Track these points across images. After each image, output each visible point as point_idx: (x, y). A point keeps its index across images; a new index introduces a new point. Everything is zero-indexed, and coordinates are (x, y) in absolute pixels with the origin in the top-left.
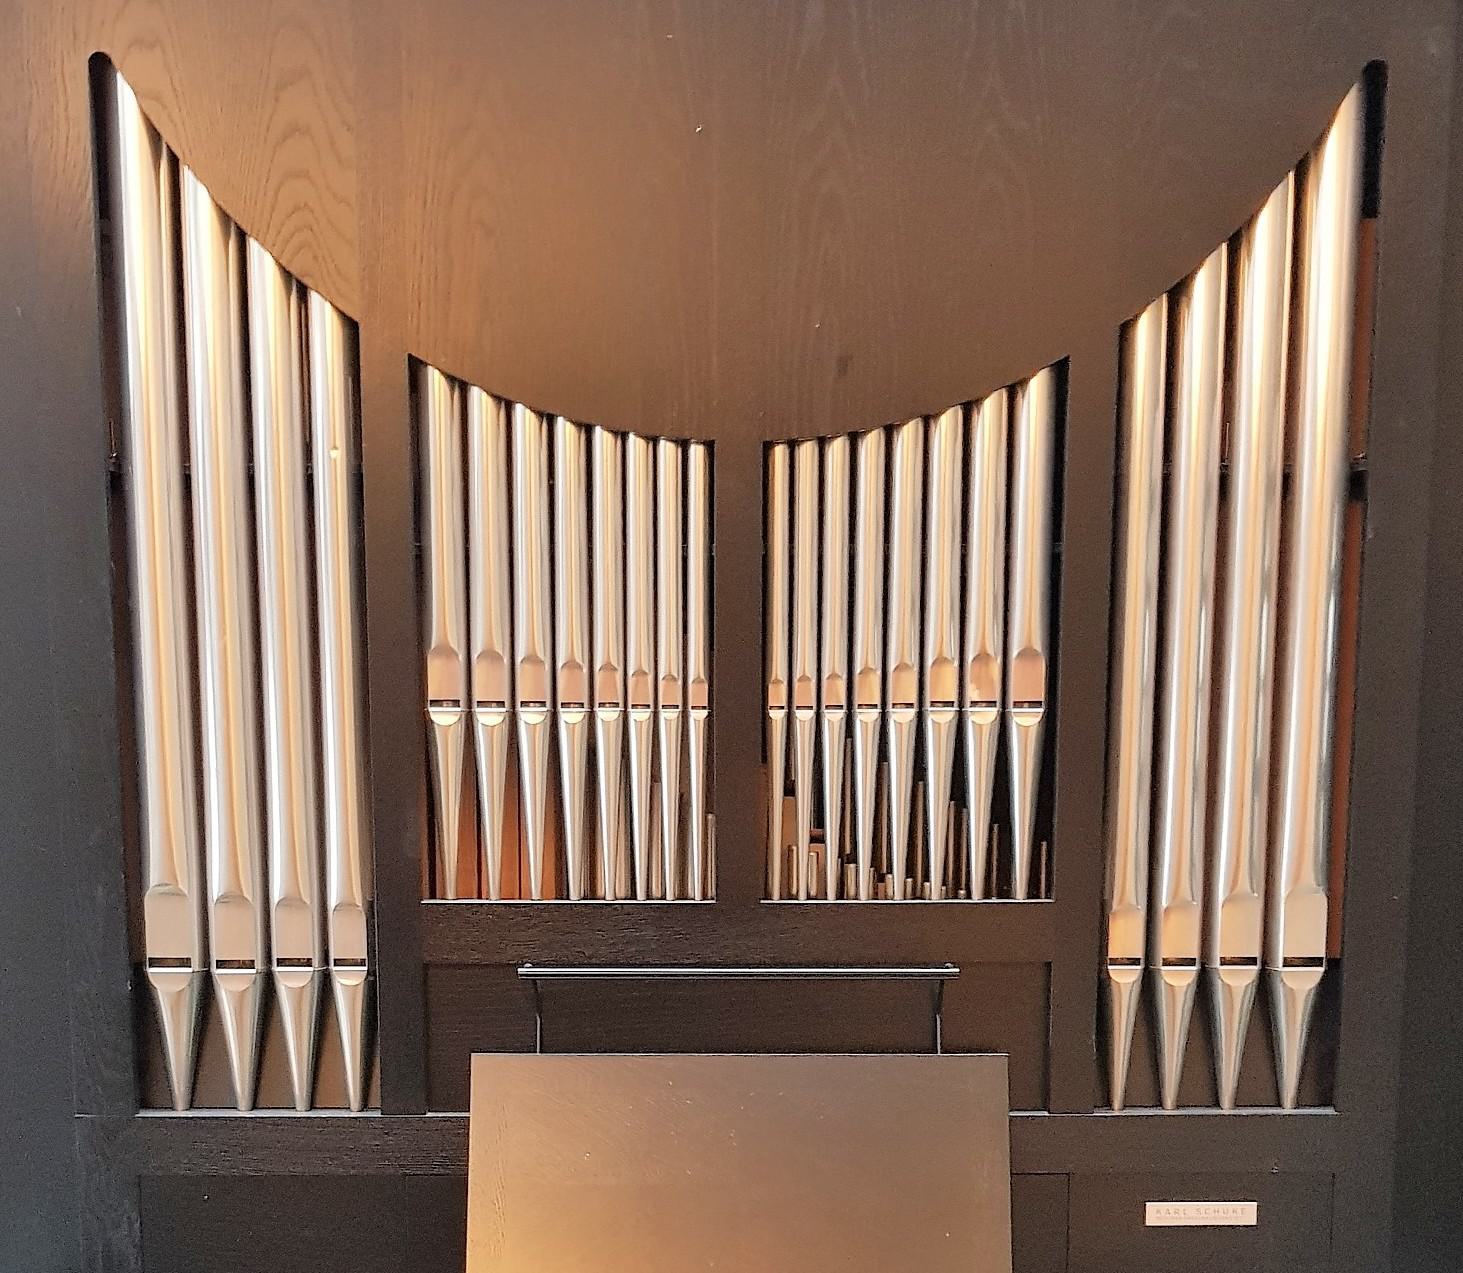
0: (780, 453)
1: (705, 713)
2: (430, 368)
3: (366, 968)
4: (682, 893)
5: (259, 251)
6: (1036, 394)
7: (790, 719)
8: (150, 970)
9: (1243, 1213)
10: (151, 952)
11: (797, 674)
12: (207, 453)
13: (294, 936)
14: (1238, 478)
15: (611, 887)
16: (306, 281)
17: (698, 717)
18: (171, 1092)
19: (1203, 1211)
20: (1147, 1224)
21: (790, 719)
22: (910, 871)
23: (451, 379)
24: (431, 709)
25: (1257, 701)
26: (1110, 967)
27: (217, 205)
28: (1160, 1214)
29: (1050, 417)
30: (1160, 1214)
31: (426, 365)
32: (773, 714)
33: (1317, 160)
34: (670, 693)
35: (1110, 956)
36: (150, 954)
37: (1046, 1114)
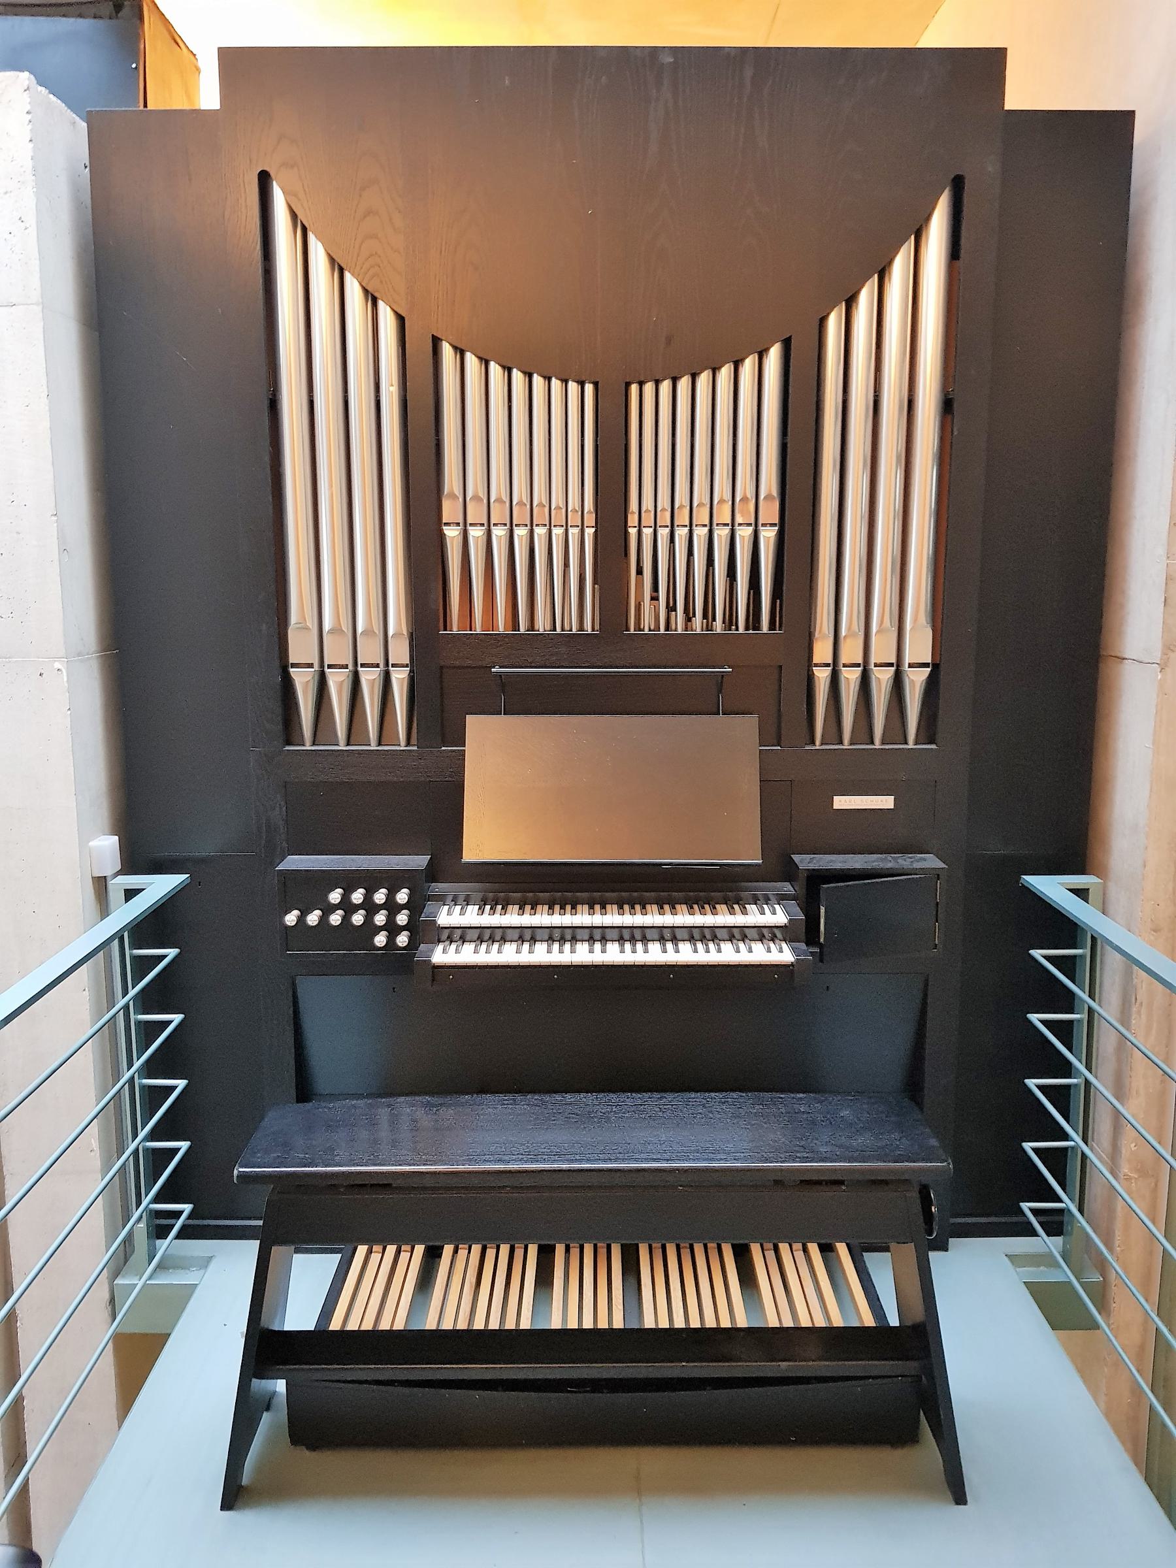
0: (634, 388)
1: (593, 530)
2: (444, 342)
3: (409, 669)
4: (581, 628)
7: (640, 533)
8: (292, 670)
9: (886, 802)
16: (376, 294)
18: (302, 736)
19: (864, 801)
21: (640, 533)
22: (705, 616)
23: (455, 348)
24: (444, 528)
26: (814, 668)
28: (842, 802)
30: (842, 802)
31: (442, 340)
34: (575, 519)
36: (291, 661)
37: (779, 748)
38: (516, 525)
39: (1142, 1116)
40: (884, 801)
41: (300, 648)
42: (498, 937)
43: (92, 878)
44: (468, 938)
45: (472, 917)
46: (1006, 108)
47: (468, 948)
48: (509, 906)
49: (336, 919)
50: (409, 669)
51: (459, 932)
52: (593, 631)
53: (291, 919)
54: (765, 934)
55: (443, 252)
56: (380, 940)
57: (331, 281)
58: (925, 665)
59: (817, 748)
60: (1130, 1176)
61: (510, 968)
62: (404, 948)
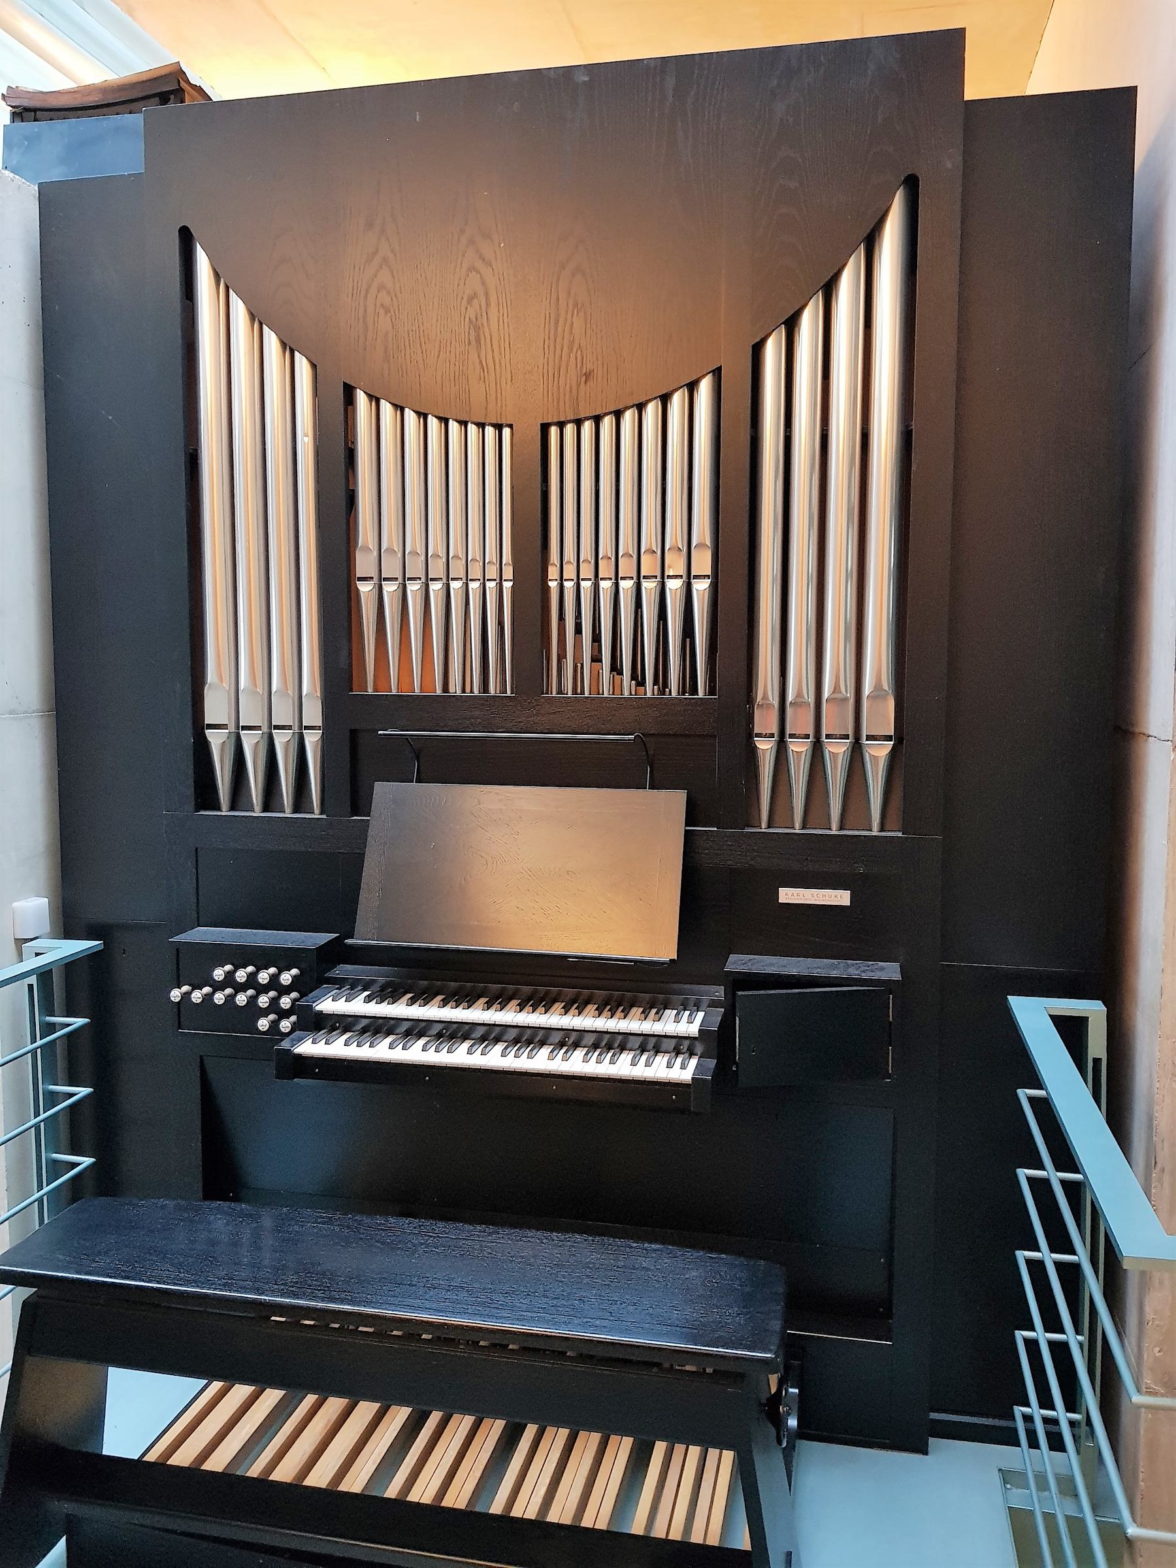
0: (554, 431)
1: (511, 583)
2: (358, 390)
3: (321, 731)
5: (269, 332)
6: (705, 388)
7: (561, 588)
8: (207, 731)
9: (841, 898)
10: (208, 720)
11: (566, 559)
12: (242, 492)
13: (283, 713)
14: (829, 565)
15: (455, 688)
16: (293, 347)
17: (507, 585)
18: (218, 799)
19: (815, 895)
20: (780, 901)
21: (561, 588)
23: (370, 397)
24: (358, 583)
25: (848, 533)
26: (755, 739)
27: (250, 312)
28: (788, 895)
29: (714, 524)
30: (788, 895)
31: (356, 388)
32: (551, 584)
33: (879, 235)
34: (492, 572)
35: (755, 732)
36: (207, 721)
37: (716, 829)
38: (621, 578)
39: (1169, 1314)
40: (839, 897)
41: (215, 709)
42: (650, 1045)
43: (15, 939)
44: (629, 1046)
45: (359, 1006)
46: (965, 99)
47: (661, 1060)
48: (666, 1010)
49: (219, 998)
50: (321, 731)
51: (653, 1040)
52: (590, 694)
53: (176, 995)
54: (679, 1046)
55: (355, 295)
56: (263, 1024)
57: (251, 335)
58: (888, 738)
59: (223, 814)
60: (1154, 1389)
61: (564, 1078)
62: (264, 1033)
